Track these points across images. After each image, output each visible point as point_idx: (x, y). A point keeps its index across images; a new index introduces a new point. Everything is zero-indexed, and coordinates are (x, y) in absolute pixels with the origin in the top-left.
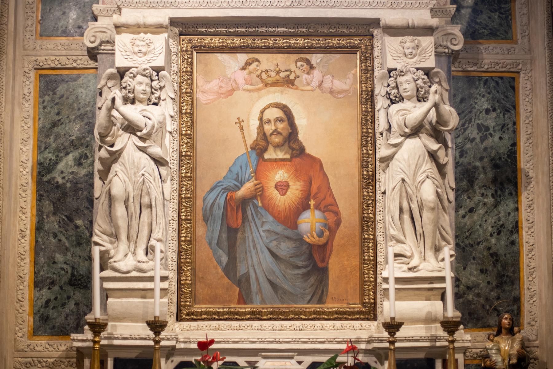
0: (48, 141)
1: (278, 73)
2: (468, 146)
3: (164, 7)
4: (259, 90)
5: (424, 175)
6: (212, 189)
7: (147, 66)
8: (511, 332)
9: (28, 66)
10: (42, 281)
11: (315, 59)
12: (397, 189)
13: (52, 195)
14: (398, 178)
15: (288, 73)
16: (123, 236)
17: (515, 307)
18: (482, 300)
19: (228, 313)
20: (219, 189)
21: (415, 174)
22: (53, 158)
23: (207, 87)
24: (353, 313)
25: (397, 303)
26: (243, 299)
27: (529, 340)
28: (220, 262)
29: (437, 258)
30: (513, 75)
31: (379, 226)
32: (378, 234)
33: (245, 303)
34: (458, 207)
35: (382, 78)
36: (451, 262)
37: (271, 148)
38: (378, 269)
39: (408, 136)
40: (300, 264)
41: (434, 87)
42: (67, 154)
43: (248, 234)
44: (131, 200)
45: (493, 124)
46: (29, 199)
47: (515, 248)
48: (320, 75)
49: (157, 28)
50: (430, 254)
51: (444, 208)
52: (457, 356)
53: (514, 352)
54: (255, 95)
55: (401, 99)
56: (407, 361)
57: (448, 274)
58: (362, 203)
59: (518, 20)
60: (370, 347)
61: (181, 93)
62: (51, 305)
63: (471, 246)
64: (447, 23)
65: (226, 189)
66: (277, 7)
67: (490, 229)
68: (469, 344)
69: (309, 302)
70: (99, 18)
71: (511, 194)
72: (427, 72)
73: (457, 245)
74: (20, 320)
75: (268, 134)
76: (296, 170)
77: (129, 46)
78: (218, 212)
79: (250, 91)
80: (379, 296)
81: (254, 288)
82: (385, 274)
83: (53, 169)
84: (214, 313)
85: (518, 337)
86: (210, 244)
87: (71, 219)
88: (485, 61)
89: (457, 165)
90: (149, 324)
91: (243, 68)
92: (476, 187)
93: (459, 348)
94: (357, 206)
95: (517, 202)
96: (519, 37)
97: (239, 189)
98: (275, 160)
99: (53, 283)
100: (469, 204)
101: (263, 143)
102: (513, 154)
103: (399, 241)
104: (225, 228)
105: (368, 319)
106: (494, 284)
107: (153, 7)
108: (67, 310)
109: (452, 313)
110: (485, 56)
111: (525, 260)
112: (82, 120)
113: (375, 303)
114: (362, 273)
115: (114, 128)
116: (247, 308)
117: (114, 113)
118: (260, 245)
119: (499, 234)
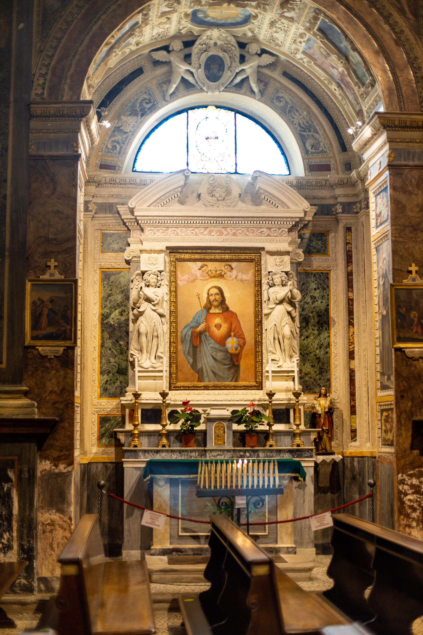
0: (106, 303)
1: (216, 271)
2: (306, 306)
3: (163, 241)
4: (207, 279)
5: (285, 322)
6: (185, 327)
7: (156, 270)
8: (325, 396)
9: (97, 267)
10: (104, 371)
11: (234, 264)
12: (272, 329)
13: (108, 330)
14: (273, 324)
15: (221, 272)
16: (145, 351)
17: (328, 384)
18: (312, 380)
19: (193, 386)
20: (189, 327)
21: (281, 322)
22: (109, 312)
23: (183, 278)
24: (251, 387)
25: (273, 382)
26: (200, 380)
27: (334, 399)
28: (189, 362)
29: (291, 361)
30: (327, 272)
31: (264, 345)
32: (263, 349)
33: (201, 382)
34: (301, 335)
35: (266, 276)
36: (297, 363)
37: (213, 308)
38: (264, 366)
39: (277, 304)
40: (227, 363)
41: (290, 283)
42: (116, 310)
43: (202, 348)
44: (149, 334)
45: (318, 296)
46: (97, 332)
47: (328, 355)
48: (236, 272)
49: (160, 251)
50: (288, 359)
51: (294, 337)
52: (300, 407)
53: (327, 405)
54: (205, 282)
55: (274, 285)
56: (277, 410)
57: (296, 369)
58: (255, 334)
59: (330, 245)
60: (260, 403)
61: (170, 282)
62: (109, 383)
63: (307, 354)
64: (296, 248)
65: (192, 327)
66: (216, 242)
67: (316, 346)
68: (306, 402)
69: (231, 381)
70: (131, 245)
71: (326, 329)
72: (287, 273)
73: (301, 354)
74: (94, 390)
75: (211, 301)
76: (225, 318)
77: (147, 260)
78: (188, 338)
79: (203, 280)
80: (264, 379)
81: (205, 375)
82: (267, 369)
83: (109, 317)
84: (187, 387)
85: (329, 398)
86: (184, 353)
87: (117, 342)
88: (314, 265)
89: (300, 315)
90: (160, 394)
91: (200, 269)
92: (310, 326)
93: (301, 404)
94: (253, 336)
95: (329, 333)
96: (331, 253)
97: (198, 327)
98: (215, 313)
99: (109, 372)
100: (306, 334)
101: (209, 305)
102: (327, 310)
103: (273, 353)
104: (191, 346)
105: (259, 389)
106: (318, 372)
107: (158, 241)
108: (116, 385)
109: (298, 387)
110: (314, 263)
111: (333, 361)
112: (122, 293)
113: (262, 382)
114: (256, 368)
115: (141, 300)
116: (202, 384)
117: (141, 293)
118: (208, 354)
119: (320, 348)
